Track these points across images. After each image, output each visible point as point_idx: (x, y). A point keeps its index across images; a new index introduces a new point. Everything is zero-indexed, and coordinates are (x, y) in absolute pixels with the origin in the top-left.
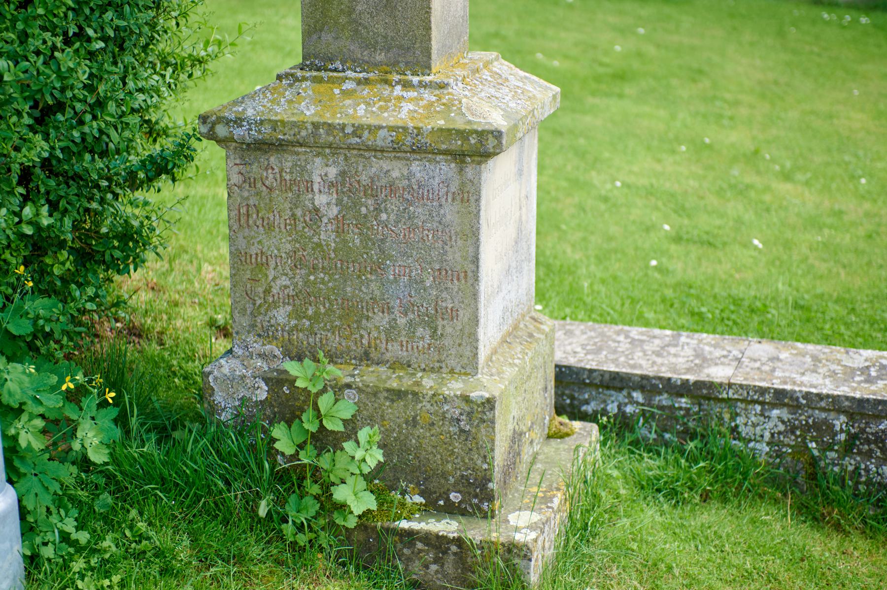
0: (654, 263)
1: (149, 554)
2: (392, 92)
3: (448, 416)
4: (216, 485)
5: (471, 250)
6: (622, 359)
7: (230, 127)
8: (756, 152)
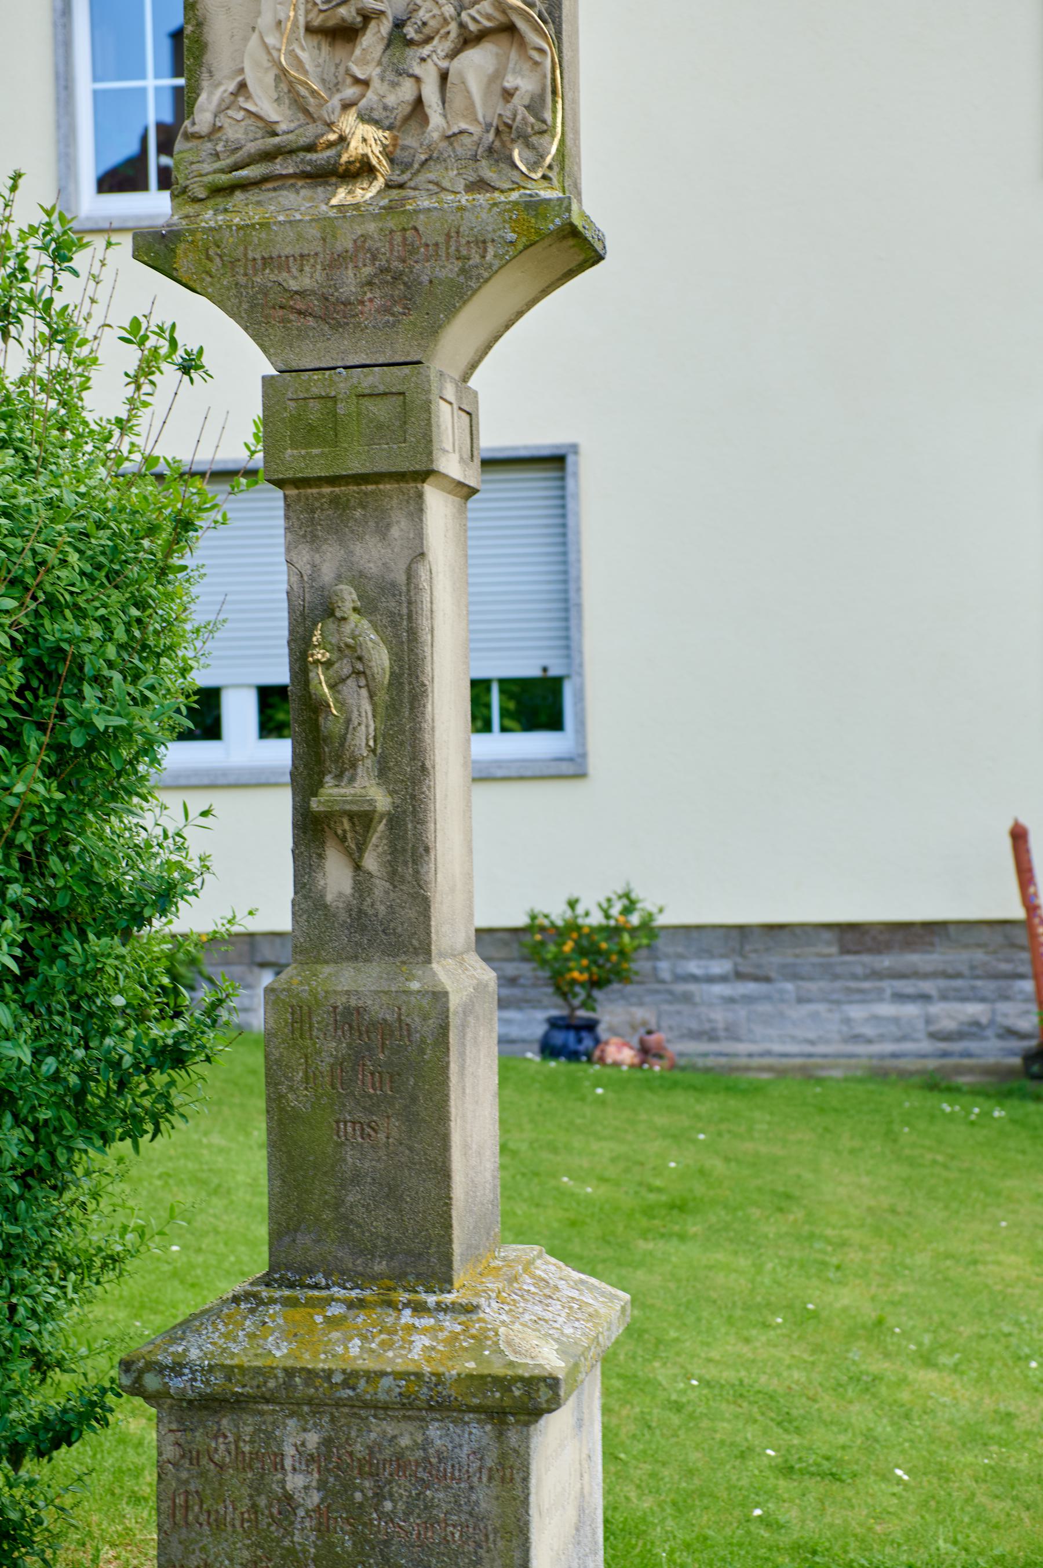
0: (758, 1512)
2: (398, 1318)
5: (517, 1554)
7: (164, 1376)
8: (880, 1323)
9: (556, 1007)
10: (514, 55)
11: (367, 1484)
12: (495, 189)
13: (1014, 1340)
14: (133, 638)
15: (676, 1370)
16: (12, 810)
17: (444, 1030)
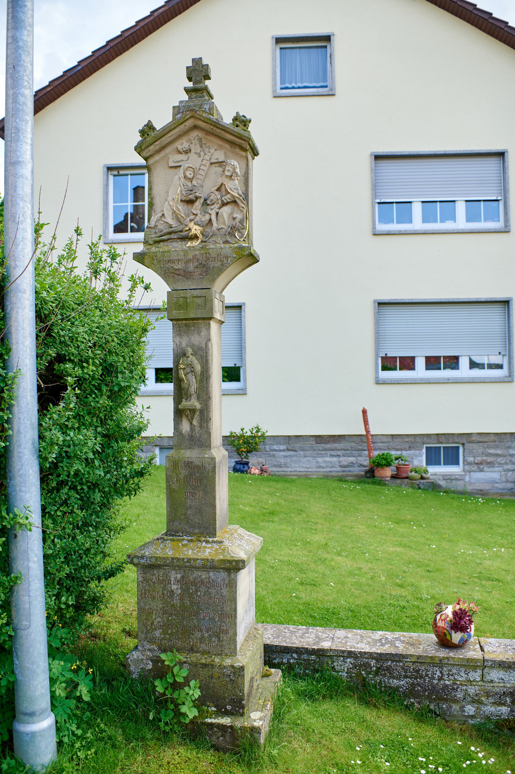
0: (294, 595)
1: (106, 738)
3: (226, 674)
4: (131, 706)
5: (233, 606)
6: (288, 640)
8: (326, 544)
9: (237, 458)
10: (236, 208)
11: (193, 588)
12: (230, 243)
13: (362, 548)
14: (131, 361)
15: (272, 557)
16: (99, 407)
17: (214, 468)
